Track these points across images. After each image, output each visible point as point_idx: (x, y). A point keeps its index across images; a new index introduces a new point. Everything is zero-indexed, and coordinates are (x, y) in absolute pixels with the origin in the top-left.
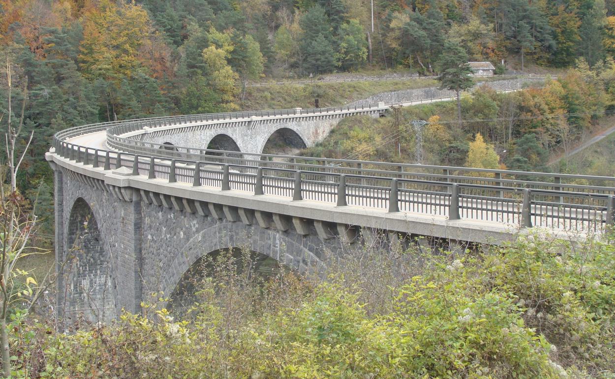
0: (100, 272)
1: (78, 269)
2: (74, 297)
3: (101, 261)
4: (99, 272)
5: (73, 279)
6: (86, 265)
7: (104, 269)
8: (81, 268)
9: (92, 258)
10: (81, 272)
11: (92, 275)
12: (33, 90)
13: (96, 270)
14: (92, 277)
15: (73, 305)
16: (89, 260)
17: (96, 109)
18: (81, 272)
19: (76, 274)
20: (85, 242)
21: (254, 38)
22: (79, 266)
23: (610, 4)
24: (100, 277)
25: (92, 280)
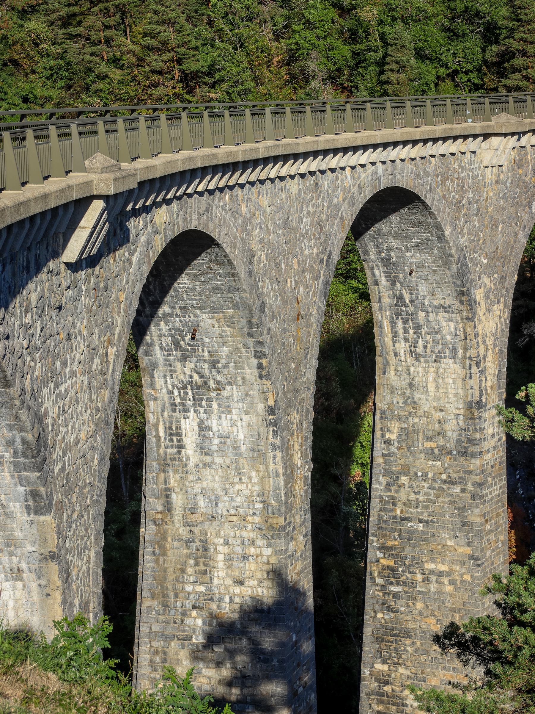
0: (220, 406)
1: (171, 393)
2: (165, 453)
3: (217, 382)
4: (215, 405)
5: (162, 415)
6: (185, 388)
7: (225, 401)
8: (176, 392)
9: (196, 372)
10: (178, 400)
11: (202, 410)
12: (393, 323)
13: (209, 399)
14: (203, 416)
15: (164, 471)
16: (191, 377)
17: (395, 424)
18: (178, 400)
19: (167, 405)
20: (171, 335)
21: (80, 606)
22: (170, 387)
23: (502, 176)
24: (220, 418)
25: (201, 422)
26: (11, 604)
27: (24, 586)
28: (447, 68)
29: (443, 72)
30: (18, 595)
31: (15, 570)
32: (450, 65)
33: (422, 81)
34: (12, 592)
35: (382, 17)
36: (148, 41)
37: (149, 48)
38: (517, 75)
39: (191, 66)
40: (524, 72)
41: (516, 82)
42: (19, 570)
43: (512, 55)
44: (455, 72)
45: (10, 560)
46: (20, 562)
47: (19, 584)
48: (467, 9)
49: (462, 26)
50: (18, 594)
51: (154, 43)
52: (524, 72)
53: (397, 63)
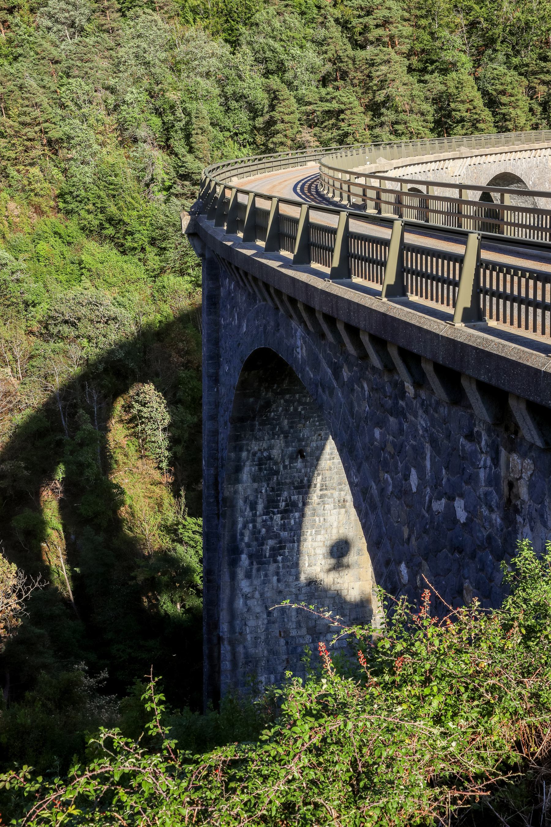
26: (335, 525)
27: (346, 512)
28: (230, 132)
29: (227, 134)
30: (341, 518)
31: (342, 501)
32: (232, 129)
33: (216, 141)
34: (337, 517)
35: (184, 98)
36: (23, 118)
37: (24, 124)
38: (279, 135)
39: (55, 134)
40: (284, 133)
41: (280, 140)
42: (344, 501)
43: (275, 123)
44: (236, 134)
45: (339, 494)
46: (346, 495)
47: (343, 510)
48: (234, 93)
49: (233, 104)
50: (341, 517)
51: (28, 119)
52: (284, 133)
53: (201, 129)
